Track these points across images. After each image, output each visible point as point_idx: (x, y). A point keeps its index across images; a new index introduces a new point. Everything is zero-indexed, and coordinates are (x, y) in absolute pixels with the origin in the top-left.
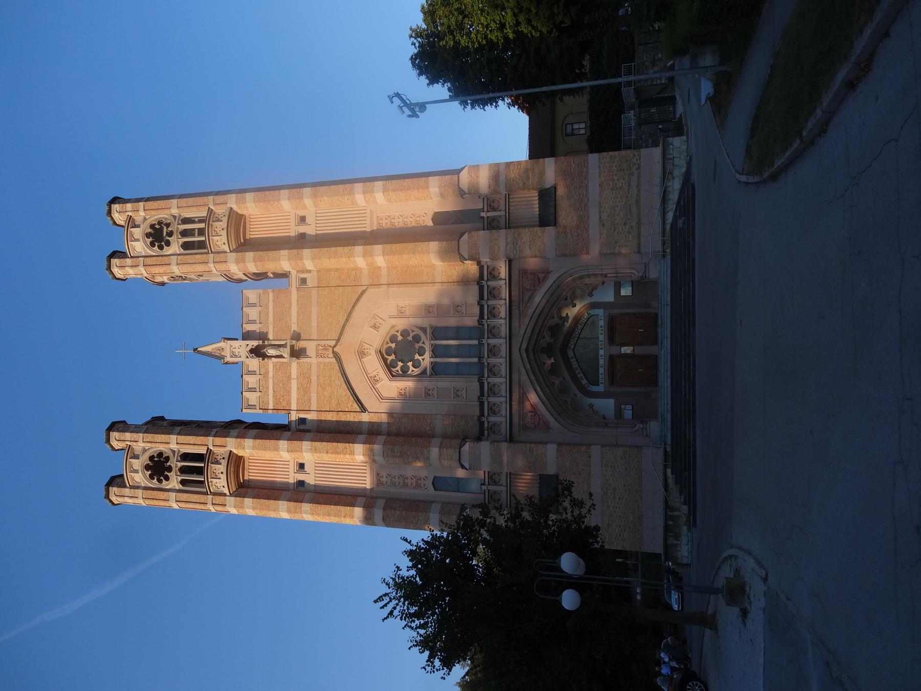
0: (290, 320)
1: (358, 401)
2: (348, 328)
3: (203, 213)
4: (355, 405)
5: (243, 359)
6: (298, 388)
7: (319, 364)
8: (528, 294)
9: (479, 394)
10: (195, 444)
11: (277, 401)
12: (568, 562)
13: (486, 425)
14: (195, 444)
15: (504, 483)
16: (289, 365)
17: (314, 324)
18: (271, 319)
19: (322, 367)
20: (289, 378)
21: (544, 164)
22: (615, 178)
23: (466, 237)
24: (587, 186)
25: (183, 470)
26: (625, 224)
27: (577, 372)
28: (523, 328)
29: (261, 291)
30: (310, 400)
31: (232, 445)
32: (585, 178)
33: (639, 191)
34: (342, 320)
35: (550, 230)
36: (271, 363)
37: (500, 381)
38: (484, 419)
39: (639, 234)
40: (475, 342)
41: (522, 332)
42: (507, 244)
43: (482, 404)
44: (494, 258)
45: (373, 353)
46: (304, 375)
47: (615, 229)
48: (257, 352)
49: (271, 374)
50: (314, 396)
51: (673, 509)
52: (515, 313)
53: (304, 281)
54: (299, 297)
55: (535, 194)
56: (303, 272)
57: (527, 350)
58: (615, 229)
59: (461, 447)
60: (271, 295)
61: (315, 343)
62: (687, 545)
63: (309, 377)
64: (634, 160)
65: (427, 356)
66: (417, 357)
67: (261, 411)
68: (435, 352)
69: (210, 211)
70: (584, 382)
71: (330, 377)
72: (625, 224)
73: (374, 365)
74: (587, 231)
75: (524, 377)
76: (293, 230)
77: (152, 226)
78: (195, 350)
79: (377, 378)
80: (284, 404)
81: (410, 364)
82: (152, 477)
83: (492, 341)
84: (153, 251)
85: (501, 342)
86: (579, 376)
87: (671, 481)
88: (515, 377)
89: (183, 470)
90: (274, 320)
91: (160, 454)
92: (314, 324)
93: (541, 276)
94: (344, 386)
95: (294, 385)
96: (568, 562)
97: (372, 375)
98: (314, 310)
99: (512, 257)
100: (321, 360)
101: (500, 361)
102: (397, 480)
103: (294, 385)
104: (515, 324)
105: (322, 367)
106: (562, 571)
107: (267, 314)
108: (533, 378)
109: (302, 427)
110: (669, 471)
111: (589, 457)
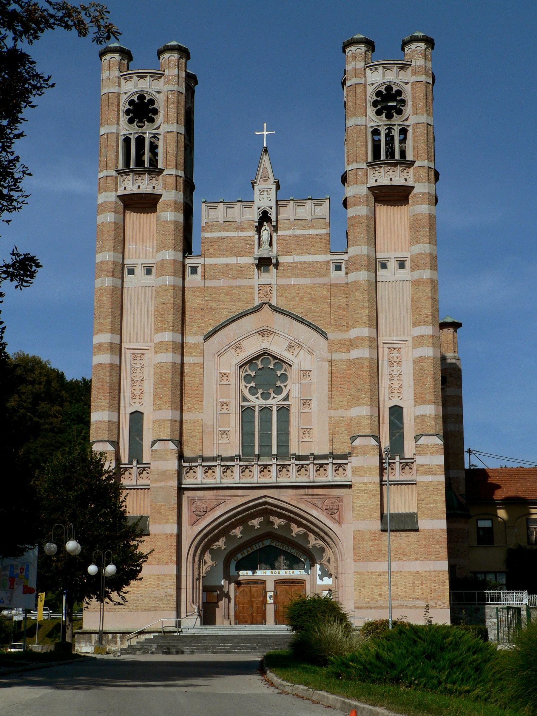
0: (298, 254)
1: (216, 331)
2: (287, 319)
3: (410, 157)
4: (211, 328)
5: (257, 204)
6: (227, 265)
7: (252, 287)
8: (319, 504)
9: (224, 455)
10: (168, 154)
11: (213, 241)
12: (111, 569)
13: (194, 464)
14: (168, 154)
15: (139, 483)
16: (251, 254)
17: (293, 281)
18: (298, 232)
19: (249, 291)
20: (238, 255)
21: (441, 519)
22: (424, 586)
23: (374, 442)
24: (417, 559)
25: (140, 140)
26: (380, 595)
27: (249, 549)
28: (288, 499)
29: (328, 220)
30: (215, 278)
31: (170, 196)
32: (426, 559)
33: (411, 608)
34: (297, 312)
35: (377, 525)
36: (252, 233)
37: (235, 477)
38: (200, 462)
39: (371, 608)
40: (274, 452)
41: (282, 498)
42: (365, 484)
43: (214, 459)
44: (355, 471)
45: (264, 346)
46: (240, 272)
47: (376, 586)
48: (265, 217)
49: (242, 234)
50: (220, 283)
51: (122, 639)
52: (301, 492)
53: (338, 268)
54: (321, 263)
55: (415, 511)
56: (346, 267)
57: (266, 503)
58: (376, 586)
59: (172, 440)
60: (323, 231)
61: (273, 282)
62: (138, 643)
63: (239, 277)
64: (439, 603)
65: (262, 402)
66: (260, 391)
67: (203, 224)
68: (265, 410)
69: (412, 163)
70: (240, 556)
71: (239, 300)
72: (380, 595)
73: (278, 347)
74: (375, 560)
75: (240, 501)
76: (378, 280)
77: (399, 93)
78: (266, 151)
79: (292, 350)
80: (211, 250)
81: (253, 374)
82: (131, 103)
83: (274, 469)
84: (372, 95)
85: (273, 477)
86: (245, 551)
87: (148, 636)
88: (240, 492)
89: (140, 140)
90: (297, 236)
91: (156, 112)
92: (293, 281)
93: (336, 516)
94: (231, 315)
95: (231, 260)
96: (111, 569)
97: (297, 350)
98: (307, 281)
99: (353, 488)
100: (256, 289)
101: (255, 477)
102: (138, 374)
103: (231, 260)
104: (290, 492)
105: (249, 291)
106: (106, 566)
107: (304, 228)
108: (239, 509)
109: (188, 270)
110: (151, 636)
111: (167, 564)
